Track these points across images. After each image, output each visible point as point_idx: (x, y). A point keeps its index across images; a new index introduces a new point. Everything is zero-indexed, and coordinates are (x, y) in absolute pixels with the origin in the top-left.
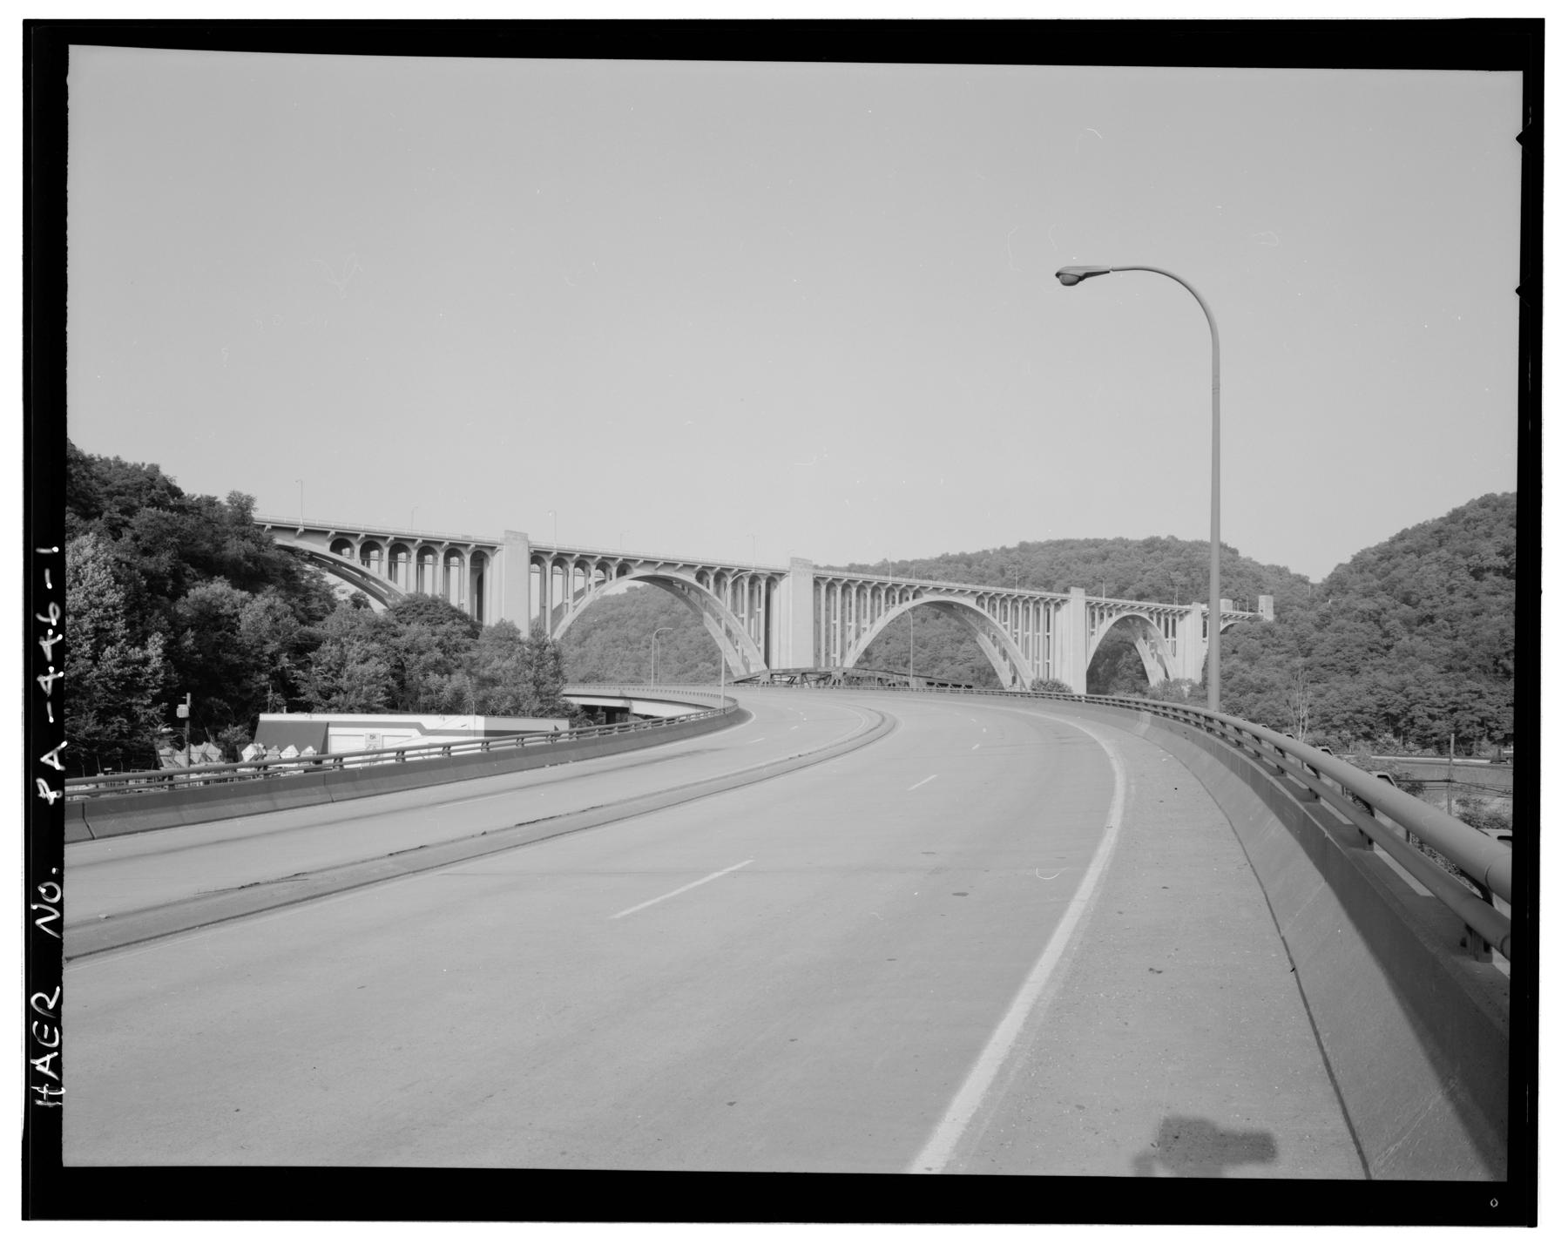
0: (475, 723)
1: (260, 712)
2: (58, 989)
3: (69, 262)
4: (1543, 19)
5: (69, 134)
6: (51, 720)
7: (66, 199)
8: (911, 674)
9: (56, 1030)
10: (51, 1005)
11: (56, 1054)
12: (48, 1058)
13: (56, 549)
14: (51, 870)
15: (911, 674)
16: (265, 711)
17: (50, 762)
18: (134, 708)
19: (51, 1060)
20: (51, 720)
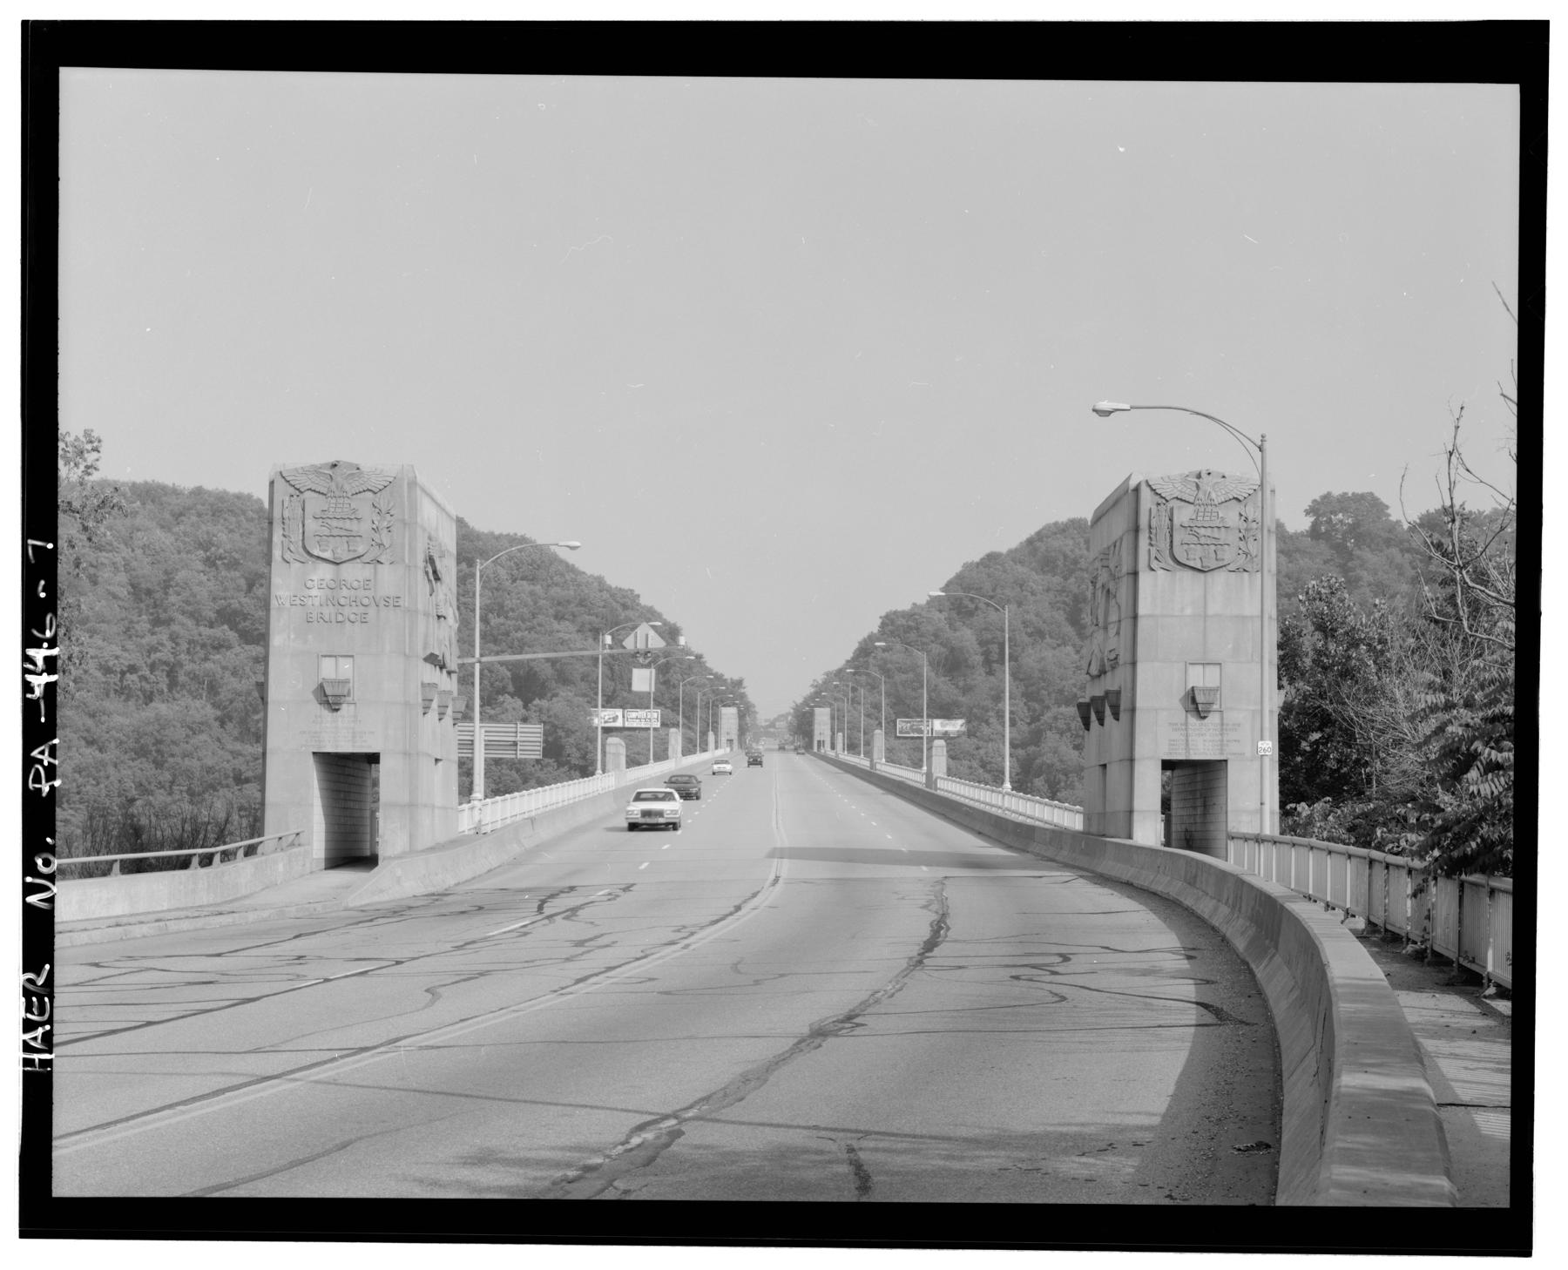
0: (1387, 881)
1: (1082, 833)
2: (47, 967)
3: (60, 345)
4: (1548, 21)
5: (61, 137)
6: (43, 720)
7: (58, 114)
8: (652, 731)
9: (46, 999)
10: (40, 982)
11: (48, 1027)
12: (40, 1031)
13: (50, 546)
14: (47, 843)
15: (652, 731)
16: (1075, 835)
18: (1353, 840)
19: (43, 1034)
20: (43, 720)
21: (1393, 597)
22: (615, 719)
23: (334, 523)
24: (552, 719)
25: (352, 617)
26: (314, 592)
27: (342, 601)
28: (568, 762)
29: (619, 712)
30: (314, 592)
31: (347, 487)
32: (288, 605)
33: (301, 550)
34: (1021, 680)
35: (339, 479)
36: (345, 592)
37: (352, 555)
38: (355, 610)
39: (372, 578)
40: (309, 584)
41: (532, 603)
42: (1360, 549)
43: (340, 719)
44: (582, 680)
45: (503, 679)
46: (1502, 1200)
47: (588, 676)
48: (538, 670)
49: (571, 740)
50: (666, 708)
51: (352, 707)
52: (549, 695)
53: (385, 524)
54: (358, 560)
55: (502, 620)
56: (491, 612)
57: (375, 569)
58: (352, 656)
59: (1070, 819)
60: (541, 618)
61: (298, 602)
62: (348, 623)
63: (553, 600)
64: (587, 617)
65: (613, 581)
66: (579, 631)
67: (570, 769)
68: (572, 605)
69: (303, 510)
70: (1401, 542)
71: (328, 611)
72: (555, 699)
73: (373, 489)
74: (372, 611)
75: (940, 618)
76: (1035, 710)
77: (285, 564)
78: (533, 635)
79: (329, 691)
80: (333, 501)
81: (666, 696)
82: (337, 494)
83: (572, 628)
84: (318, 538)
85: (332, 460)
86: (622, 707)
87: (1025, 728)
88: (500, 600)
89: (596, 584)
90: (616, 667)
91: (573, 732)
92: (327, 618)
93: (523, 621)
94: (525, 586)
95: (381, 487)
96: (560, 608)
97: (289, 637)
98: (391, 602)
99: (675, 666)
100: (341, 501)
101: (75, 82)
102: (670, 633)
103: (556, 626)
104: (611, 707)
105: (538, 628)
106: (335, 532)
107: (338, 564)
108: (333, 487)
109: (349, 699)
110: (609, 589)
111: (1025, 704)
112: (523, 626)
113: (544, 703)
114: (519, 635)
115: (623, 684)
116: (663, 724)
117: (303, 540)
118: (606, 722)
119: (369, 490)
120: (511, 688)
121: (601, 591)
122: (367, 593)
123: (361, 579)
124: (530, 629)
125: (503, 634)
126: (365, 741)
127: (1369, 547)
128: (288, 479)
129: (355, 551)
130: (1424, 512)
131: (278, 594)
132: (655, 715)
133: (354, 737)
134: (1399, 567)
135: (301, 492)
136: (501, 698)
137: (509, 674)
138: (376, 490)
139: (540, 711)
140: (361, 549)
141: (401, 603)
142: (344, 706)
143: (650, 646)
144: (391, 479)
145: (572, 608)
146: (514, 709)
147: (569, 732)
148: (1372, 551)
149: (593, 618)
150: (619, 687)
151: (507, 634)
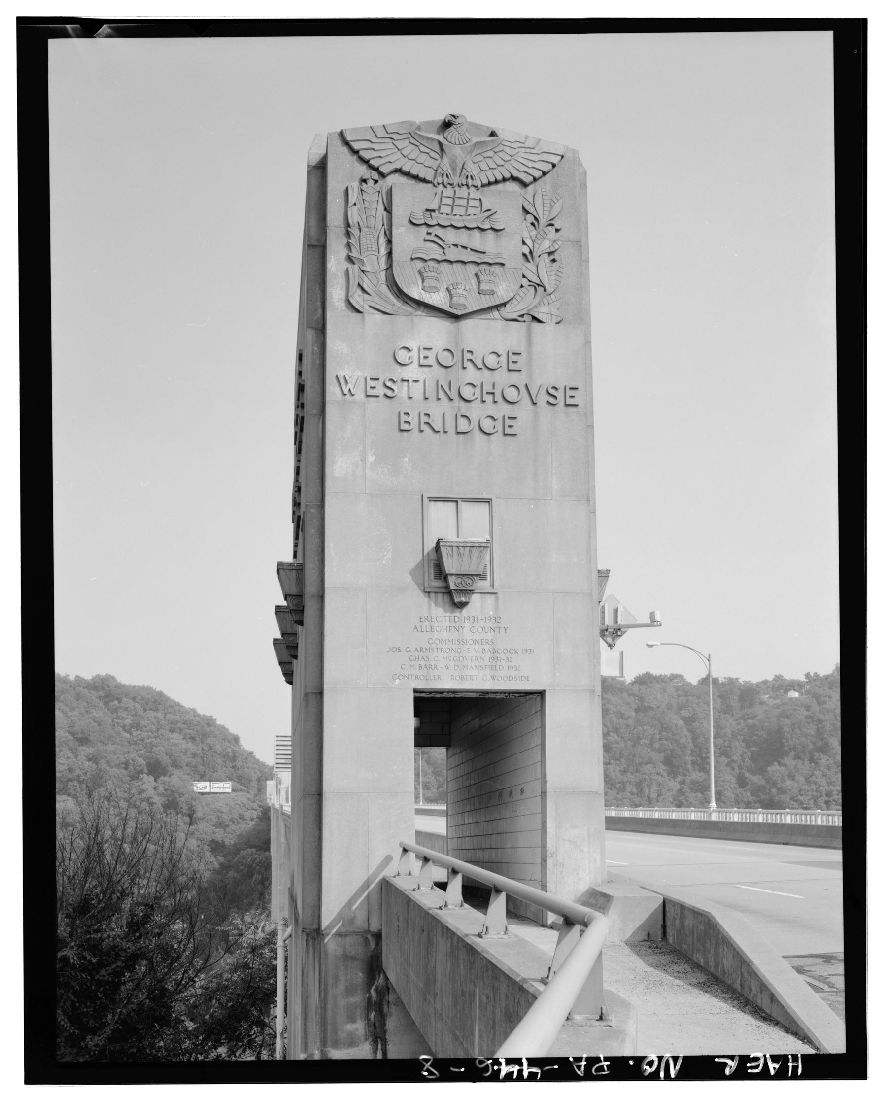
17: (583, 1069)
21: (627, 719)
22: (205, 788)
23: (450, 236)
24: (171, 788)
25: (487, 425)
27: (467, 392)
28: (181, 812)
29: (208, 784)
30: (412, 372)
31: (473, 169)
32: (360, 396)
33: (384, 289)
34: (431, 765)
35: (457, 151)
36: (471, 374)
37: (487, 302)
38: (491, 409)
40: (402, 356)
41: (156, 723)
42: (606, 694)
43: (467, 625)
44: (187, 765)
45: (141, 765)
47: (190, 763)
48: (161, 760)
49: (183, 799)
50: (234, 781)
51: (490, 599)
52: (168, 774)
53: (546, 245)
54: (496, 314)
55: (139, 732)
56: (132, 728)
57: (529, 333)
58: (488, 501)
60: (162, 731)
61: (380, 391)
62: (478, 435)
63: (169, 721)
64: (188, 731)
65: (201, 711)
66: (183, 739)
67: (183, 816)
68: (180, 724)
69: (388, 210)
70: (628, 691)
71: (440, 411)
72: (172, 776)
73: (523, 176)
74: (524, 411)
76: (439, 782)
77: (355, 315)
78: (158, 740)
79: (450, 566)
80: (449, 192)
81: (235, 774)
82: (456, 180)
83: (181, 737)
84: (419, 265)
85: (441, 116)
86: (210, 781)
87: (435, 791)
88: (137, 721)
89: (192, 712)
90: (205, 759)
91: (183, 795)
92: (438, 426)
93: (152, 733)
94: (152, 714)
96: (172, 726)
97: (363, 460)
98: (560, 395)
99: (239, 758)
100: (463, 192)
102: (234, 740)
103: (170, 735)
104: (204, 781)
105: (161, 737)
106: (453, 254)
107: (456, 318)
108: (446, 167)
109: (482, 585)
110: (199, 716)
111: (435, 778)
112: (152, 735)
113: (166, 779)
114: (150, 740)
115: (209, 768)
116: (233, 790)
117: (390, 267)
118: (200, 789)
119: (513, 178)
120: (146, 770)
121: (195, 716)
122: (515, 378)
124: (156, 737)
125: (140, 740)
126: (517, 668)
127: (611, 693)
128: (356, 146)
130: (637, 675)
131: (341, 374)
132: (228, 785)
134: (628, 703)
135: (383, 175)
136: (141, 776)
137: (144, 762)
138: (527, 179)
139: (164, 783)
140: (503, 291)
142: (475, 600)
143: (619, 622)
144: (556, 159)
145: (179, 725)
146: (149, 782)
147: (181, 795)
148: (613, 695)
149: (191, 731)
150: (207, 770)
151: (143, 740)
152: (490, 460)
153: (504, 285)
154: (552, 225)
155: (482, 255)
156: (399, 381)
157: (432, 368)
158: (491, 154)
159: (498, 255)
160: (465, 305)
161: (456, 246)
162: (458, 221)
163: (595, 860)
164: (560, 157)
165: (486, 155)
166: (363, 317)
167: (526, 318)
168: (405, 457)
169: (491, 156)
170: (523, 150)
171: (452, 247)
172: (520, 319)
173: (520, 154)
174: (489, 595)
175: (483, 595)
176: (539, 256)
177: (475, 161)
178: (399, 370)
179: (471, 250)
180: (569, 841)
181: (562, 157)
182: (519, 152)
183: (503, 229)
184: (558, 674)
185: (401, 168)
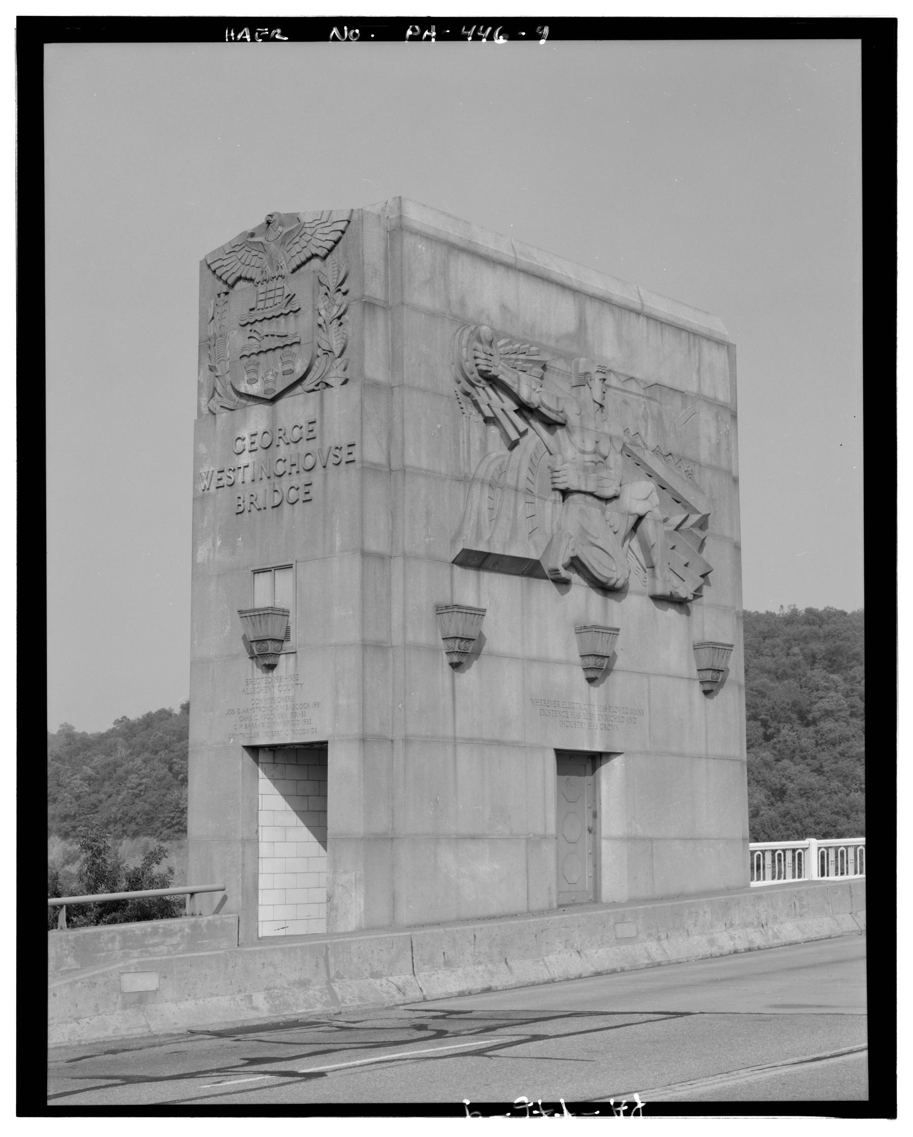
26: (245, 459)
39: (317, 417)
46: (855, 46)
51: (292, 657)
54: (299, 389)
58: (290, 567)
59: (507, 340)
75: (92, 906)
95: (336, 235)
101: (53, 53)
123: (302, 422)
129: (292, 372)
132: (708, 916)
133: (294, 714)
141: (356, 456)
152: (294, 527)
153: (300, 362)
154: (339, 290)
155: (285, 338)
156: (237, 469)
157: (257, 451)
158: (297, 239)
159: (295, 336)
160: (272, 389)
161: (267, 336)
162: (269, 312)
163: (360, 905)
164: (346, 222)
165: (294, 242)
166: (215, 418)
167: (320, 386)
168: (239, 537)
169: (298, 241)
170: (320, 226)
171: (265, 338)
172: (316, 388)
173: (318, 232)
174: (291, 655)
175: (287, 655)
176: (331, 323)
177: (241, 284)
178: (237, 459)
179: (278, 336)
180: (342, 886)
181: (349, 222)
182: (316, 230)
183: (299, 309)
184: (337, 725)
185: (241, 276)
